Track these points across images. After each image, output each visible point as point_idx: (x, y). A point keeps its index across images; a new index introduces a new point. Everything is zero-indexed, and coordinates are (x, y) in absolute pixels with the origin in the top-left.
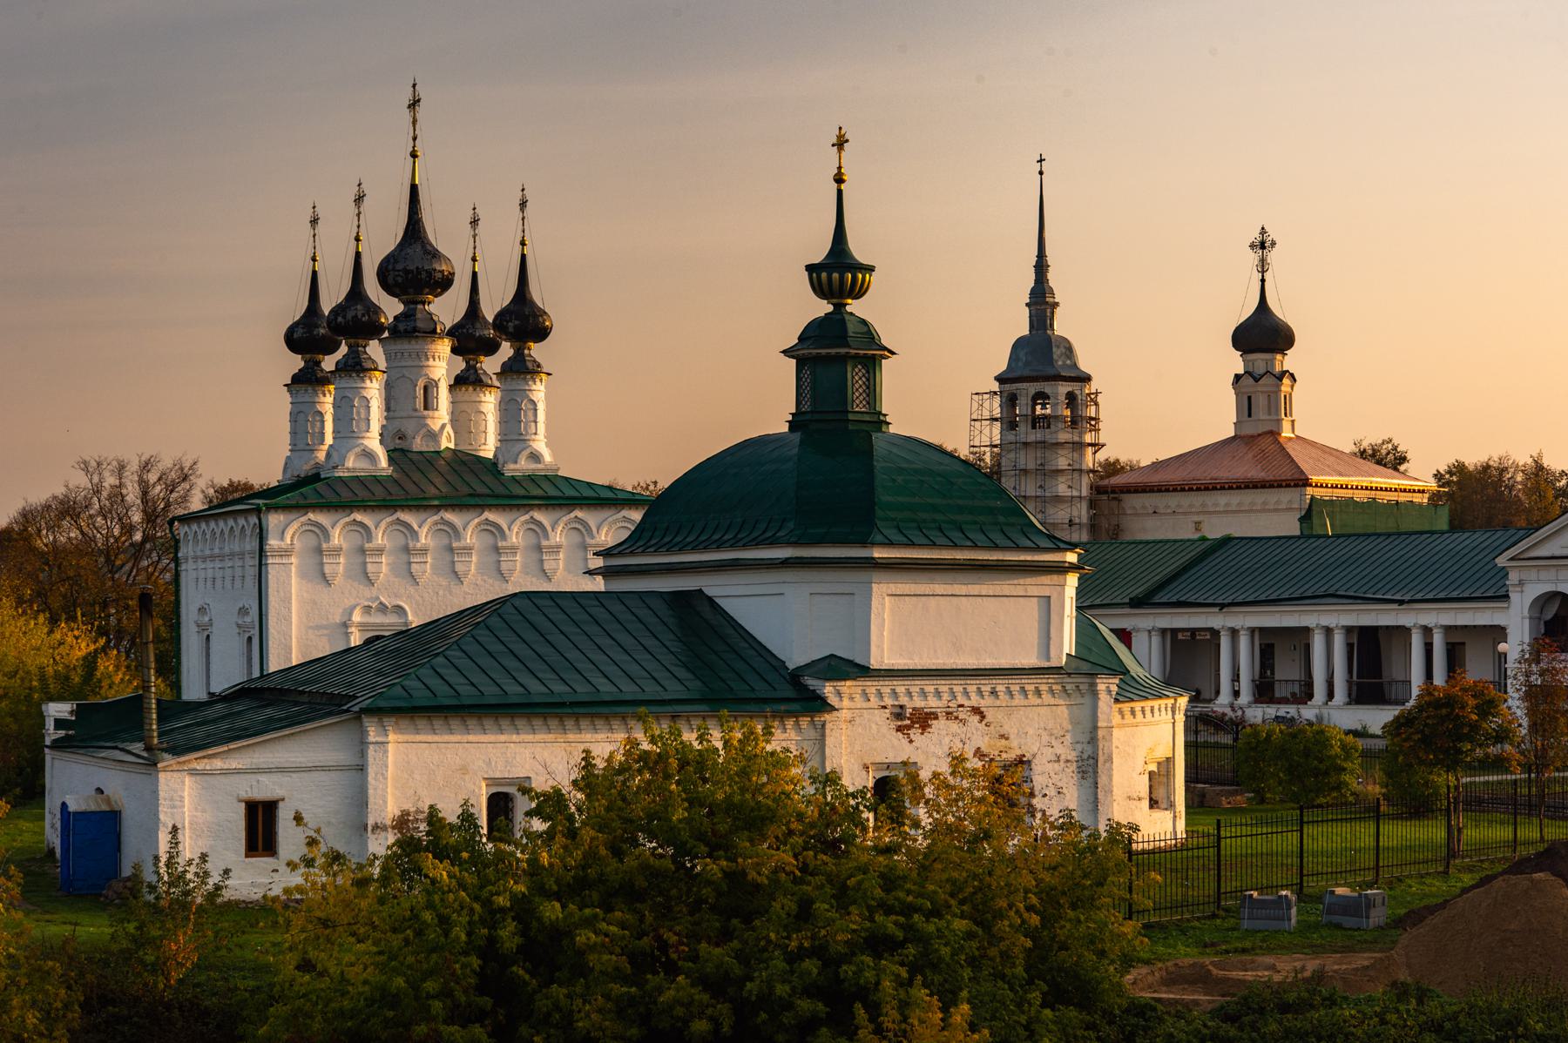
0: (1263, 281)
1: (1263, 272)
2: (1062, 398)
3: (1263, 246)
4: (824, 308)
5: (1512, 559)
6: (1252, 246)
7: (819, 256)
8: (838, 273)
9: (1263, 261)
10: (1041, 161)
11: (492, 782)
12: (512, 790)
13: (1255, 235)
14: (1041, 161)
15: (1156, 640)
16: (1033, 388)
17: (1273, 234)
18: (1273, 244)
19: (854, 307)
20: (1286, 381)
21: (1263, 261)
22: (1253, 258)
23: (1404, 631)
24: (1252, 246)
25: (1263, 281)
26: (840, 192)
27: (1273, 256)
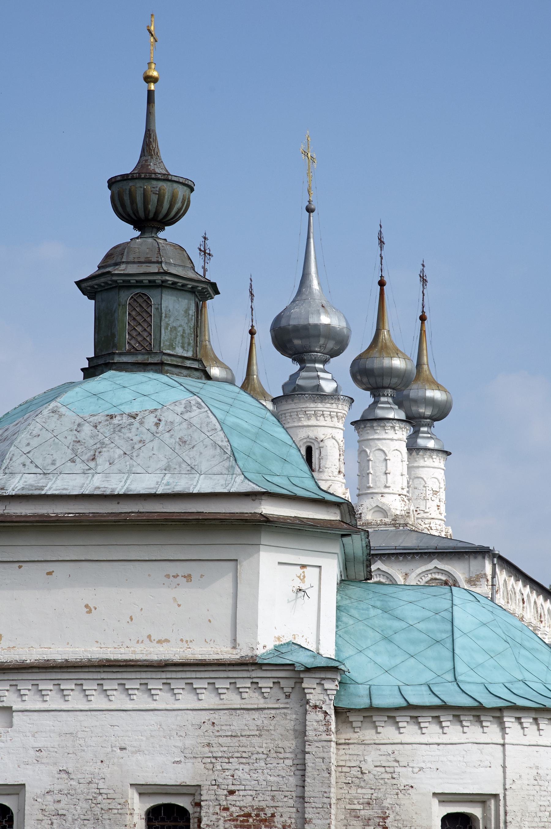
4: (127, 232)
11: (144, 790)
12: (183, 802)
19: (169, 234)
26: (150, 94)
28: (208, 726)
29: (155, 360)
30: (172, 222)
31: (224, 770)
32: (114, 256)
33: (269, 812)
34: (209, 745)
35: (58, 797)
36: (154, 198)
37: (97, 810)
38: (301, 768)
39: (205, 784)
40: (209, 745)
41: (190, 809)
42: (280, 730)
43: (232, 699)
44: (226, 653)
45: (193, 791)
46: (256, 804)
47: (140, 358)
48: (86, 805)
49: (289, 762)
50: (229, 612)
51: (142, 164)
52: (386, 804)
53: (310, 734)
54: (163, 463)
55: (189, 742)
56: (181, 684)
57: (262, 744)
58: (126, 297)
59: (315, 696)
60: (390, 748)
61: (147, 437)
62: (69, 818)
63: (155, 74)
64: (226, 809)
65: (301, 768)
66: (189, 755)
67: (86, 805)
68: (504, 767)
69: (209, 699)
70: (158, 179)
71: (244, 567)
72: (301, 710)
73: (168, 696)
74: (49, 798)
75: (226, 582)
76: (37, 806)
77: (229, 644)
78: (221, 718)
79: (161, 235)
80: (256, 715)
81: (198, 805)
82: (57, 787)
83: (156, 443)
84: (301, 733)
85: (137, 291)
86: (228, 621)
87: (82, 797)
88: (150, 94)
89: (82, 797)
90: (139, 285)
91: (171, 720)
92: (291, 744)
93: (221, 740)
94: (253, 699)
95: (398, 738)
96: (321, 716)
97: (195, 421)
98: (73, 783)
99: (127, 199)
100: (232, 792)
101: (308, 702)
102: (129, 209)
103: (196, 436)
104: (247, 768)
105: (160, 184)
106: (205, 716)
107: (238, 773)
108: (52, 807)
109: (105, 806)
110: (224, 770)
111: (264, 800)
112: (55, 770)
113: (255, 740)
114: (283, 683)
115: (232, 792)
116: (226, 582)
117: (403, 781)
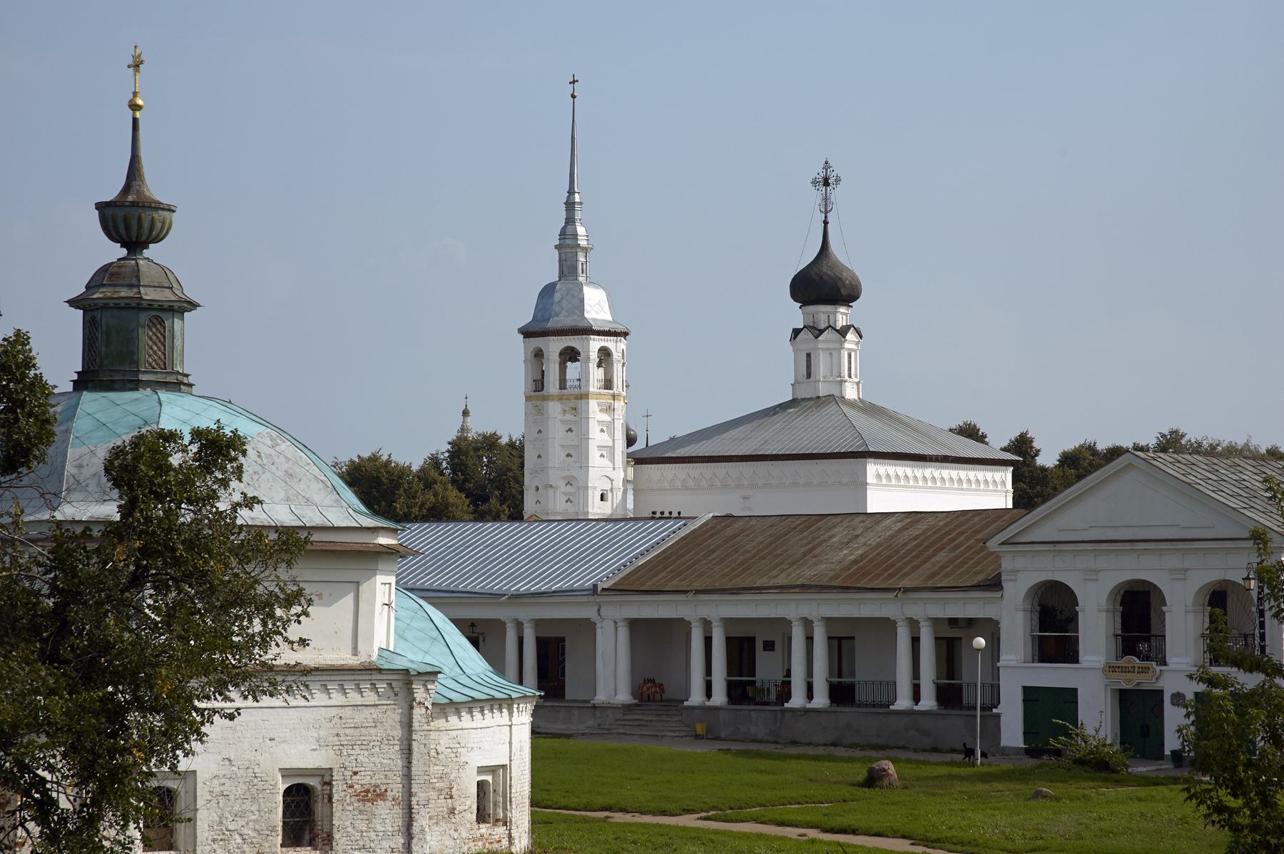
0: (826, 223)
1: (826, 212)
2: (594, 355)
3: (826, 183)
4: (116, 252)
5: (1003, 543)
6: (815, 182)
7: (111, 192)
8: (130, 219)
9: (826, 199)
10: (574, 82)
11: (286, 773)
12: (313, 782)
13: (817, 171)
14: (574, 82)
15: (623, 633)
16: (554, 346)
17: (837, 169)
18: (838, 180)
19: (152, 251)
20: (851, 336)
21: (826, 199)
22: (816, 195)
23: (887, 626)
24: (815, 182)
25: (826, 223)
26: (135, 121)
27: (836, 194)
28: (336, 720)
29: (171, 379)
30: (157, 240)
31: (349, 755)
32: (106, 275)
33: (383, 788)
34: (338, 735)
35: (223, 781)
36: (158, 225)
37: (254, 791)
38: (408, 752)
39: (336, 767)
40: (338, 735)
41: (319, 787)
42: (390, 722)
43: (354, 697)
44: (343, 657)
45: (326, 776)
46: (373, 782)
47: (160, 378)
48: (245, 787)
49: (397, 748)
50: (350, 625)
51: (127, 189)
52: (452, 777)
53: (416, 725)
54: (282, 495)
55: (323, 733)
56: (318, 685)
57: (380, 733)
58: (144, 317)
59: (420, 694)
60: (454, 733)
61: (257, 468)
62: (232, 798)
63: (140, 102)
64: (352, 787)
65: (408, 752)
66: (322, 744)
67: (245, 787)
68: (510, 743)
69: (337, 698)
70: (163, 209)
71: (364, 588)
72: (406, 706)
73: (324, 696)
74: (215, 781)
75: (349, 600)
76: (207, 789)
77: (349, 650)
78: (348, 712)
79: (146, 253)
80: (372, 710)
81: (330, 784)
82: (222, 773)
83: (266, 476)
84: (408, 725)
85: (154, 313)
86: (349, 633)
87: (241, 780)
88: (135, 121)
89: (241, 780)
90: (161, 308)
91: (309, 715)
92: (398, 733)
93: (347, 731)
94: (370, 697)
95: (460, 725)
96: (423, 710)
97: (287, 453)
98: (235, 769)
99: (134, 223)
100: (355, 773)
101: (414, 699)
102: (134, 234)
103: (297, 469)
104: (366, 753)
105: (166, 213)
106: (334, 711)
107: (360, 758)
108: (217, 790)
109: (261, 787)
110: (349, 755)
111: (379, 779)
112: (220, 758)
113: (372, 731)
114: (394, 684)
115: (355, 773)
116: (349, 600)
117: (463, 759)
